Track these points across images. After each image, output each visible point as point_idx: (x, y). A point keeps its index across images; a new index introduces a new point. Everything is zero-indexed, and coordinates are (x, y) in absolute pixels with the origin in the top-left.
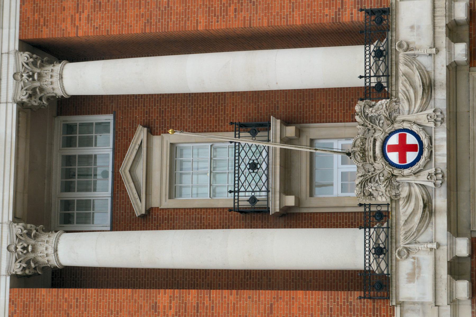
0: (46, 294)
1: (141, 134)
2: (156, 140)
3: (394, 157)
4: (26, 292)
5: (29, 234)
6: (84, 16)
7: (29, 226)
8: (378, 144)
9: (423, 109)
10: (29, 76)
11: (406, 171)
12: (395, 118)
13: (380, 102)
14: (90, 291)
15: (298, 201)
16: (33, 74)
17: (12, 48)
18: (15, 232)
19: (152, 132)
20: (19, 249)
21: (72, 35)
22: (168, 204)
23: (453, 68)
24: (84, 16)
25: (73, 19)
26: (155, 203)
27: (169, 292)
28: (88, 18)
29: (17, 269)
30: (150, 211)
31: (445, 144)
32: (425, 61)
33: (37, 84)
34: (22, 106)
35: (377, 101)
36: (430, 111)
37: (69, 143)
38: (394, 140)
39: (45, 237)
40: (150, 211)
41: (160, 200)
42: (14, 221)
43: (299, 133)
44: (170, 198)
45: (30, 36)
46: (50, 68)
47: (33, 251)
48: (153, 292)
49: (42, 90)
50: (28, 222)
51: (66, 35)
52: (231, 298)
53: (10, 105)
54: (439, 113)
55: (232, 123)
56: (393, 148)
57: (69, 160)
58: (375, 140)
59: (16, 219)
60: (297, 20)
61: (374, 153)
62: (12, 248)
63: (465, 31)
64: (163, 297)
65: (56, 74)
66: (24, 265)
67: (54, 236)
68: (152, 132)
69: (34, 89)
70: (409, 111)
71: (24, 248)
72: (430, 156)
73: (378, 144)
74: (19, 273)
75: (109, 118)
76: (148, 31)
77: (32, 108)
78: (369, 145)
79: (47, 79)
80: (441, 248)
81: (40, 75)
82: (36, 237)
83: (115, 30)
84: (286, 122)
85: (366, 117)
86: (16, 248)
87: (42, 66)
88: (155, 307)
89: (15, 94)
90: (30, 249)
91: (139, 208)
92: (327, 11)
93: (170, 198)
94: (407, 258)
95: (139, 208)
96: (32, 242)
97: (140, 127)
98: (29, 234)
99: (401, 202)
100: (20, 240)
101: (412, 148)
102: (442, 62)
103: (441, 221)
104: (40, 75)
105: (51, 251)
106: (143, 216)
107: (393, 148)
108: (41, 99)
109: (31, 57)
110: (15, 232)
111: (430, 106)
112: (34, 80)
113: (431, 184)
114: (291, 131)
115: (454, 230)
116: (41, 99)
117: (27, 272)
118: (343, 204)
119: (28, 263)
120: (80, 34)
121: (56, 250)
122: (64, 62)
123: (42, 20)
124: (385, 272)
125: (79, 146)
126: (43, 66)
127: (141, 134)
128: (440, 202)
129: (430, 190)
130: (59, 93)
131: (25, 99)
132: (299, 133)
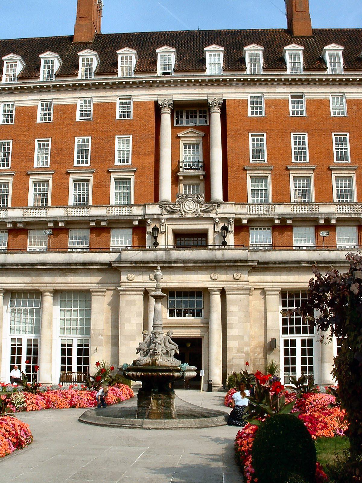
2: (201, 139)
15: (181, 180)
29: (159, 102)
43: (201, 180)
82: (169, 107)
98: (219, 104)
114: (201, 177)
132: (201, 180)
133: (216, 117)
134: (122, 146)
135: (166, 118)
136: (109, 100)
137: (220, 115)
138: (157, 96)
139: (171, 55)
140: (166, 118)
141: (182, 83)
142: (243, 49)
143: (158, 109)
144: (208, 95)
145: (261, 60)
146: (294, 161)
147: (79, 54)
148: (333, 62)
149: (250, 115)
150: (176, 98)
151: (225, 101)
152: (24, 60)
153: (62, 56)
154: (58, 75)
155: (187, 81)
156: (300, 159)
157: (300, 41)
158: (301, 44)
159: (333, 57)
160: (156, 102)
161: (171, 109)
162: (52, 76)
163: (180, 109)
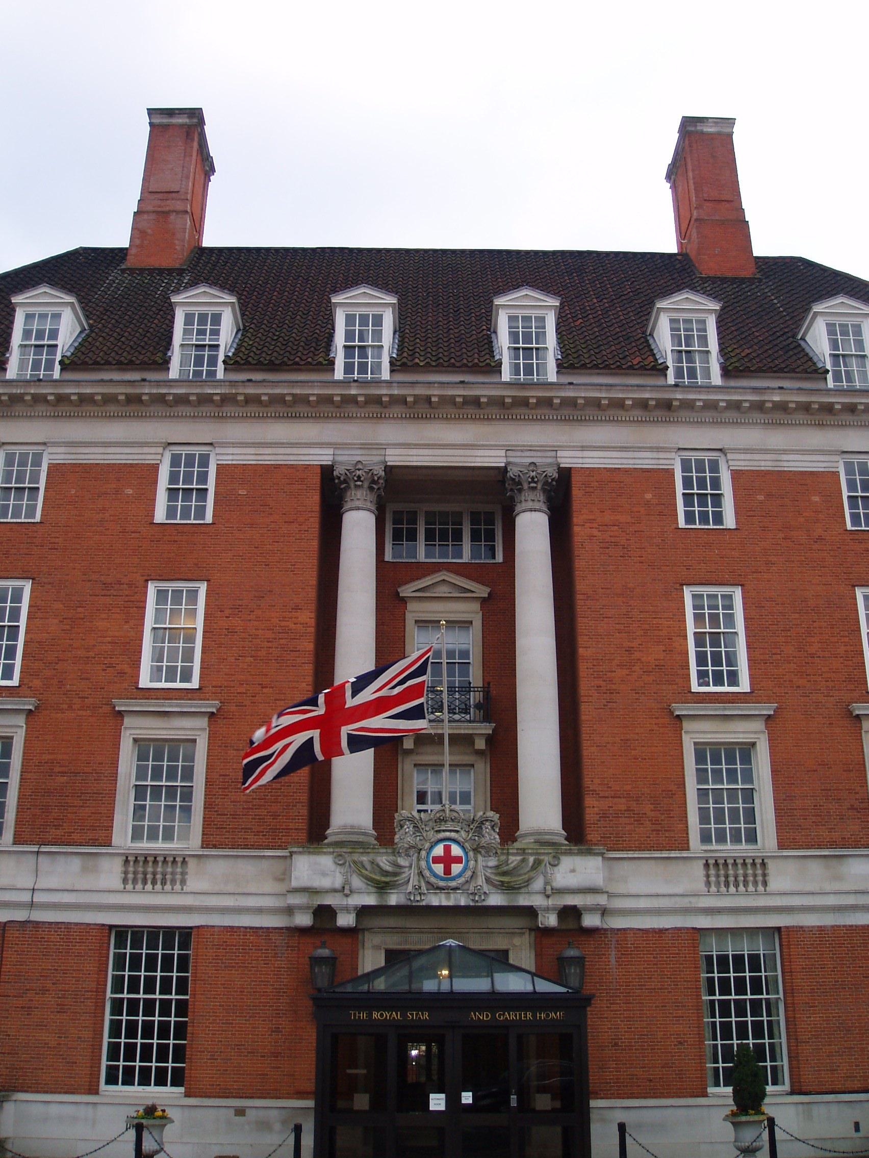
0: (314, 499)
1: (483, 591)
2: (476, 606)
3: (439, 851)
4: (316, 480)
5: (373, 482)
6: (595, 532)
7: (381, 481)
8: (453, 835)
9: (488, 880)
10: (533, 478)
11: (423, 864)
12: (480, 852)
13: (497, 837)
14: (315, 544)
15: (409, 752)
16: (535, 482)
17: (387, 459)
18: (549, 470)
19: (484, 601)
20: (358, 473)
21: (575, 520)
22: (410, 619)
23: (531, 912)
24: (595, 532)
25: (592, 521)
26: (411, 606)
27: (313, 622)
28: (591, 537)
29: (339, 471)
30: (404, 601)
31: (451, 903)
32: (538, 884)
33: (526, 486)
34: (504, 470)
35: (498, 834)
36: (486, 888)
37: (475, 518)
38: (456, 851)
39: (372, 497)
40: (404, 601)
41: (415, 612)
42: (386, 467)
43: (479, 753)
44: (416, 622)
45: (575, 479)
46: (542, 498)
47: (356, 486)
48: (313, 607)
49: (520, 491)
50: (386, 481)
51: (575, 514)
52: (304, 685)
53: (331, 458)
54: (483, 897)
55: (489, 684)
56: (447, 849)
57: (457, 519)
58: (457, 831)
59: (389, 469)
60: (589, 751)
61: (444, 831)
62: (360, 466)
63: (571, 925)
64: (308, 617)
65: (537, 505)
66: (342, 479)
67: (373, 508)
68: (484, 601)
69: (520, 483)
70: (487, 867)
71: (359, 477)
72: (439, 888)
73: (453, 835)
74: (335, 473)
75: (500, 558)
76: (578, 597)
77: (503, 482)
78: (449, 826)
79: (530, 495)
80: (345, 899)
81: (534, 488)
82: (371, 489)
83: (581, 563)
84: (490, 739)
85: (482, 823)
86: (359, 470)
87: (544, 490)
88: (297, 608)
89: (341, 463)
90: (359, 483)
91: (406, 591)
92: (597, 781)
93: (416, 622)
94: (336, 863)
95: (406, 591)
96: (366, 485)
97: (488, 590)
98: (373, 482)
99: (391, 858)
100: (367, 473)
101: (447, 871)
102: (537, 901)
103: (371, 900)
104: (534, 488)
105: (530, 505)
106: (398, 593)
107: (447, 849)
108: (512, 490)
109: (553, 480)
110: (549, 470)
111: (491, 887)
112: (530, 483)
113: (410, 888)
114: (480, 744)
115: (363, 912)
116: (512, 490)
117: (337, 481)
118: (405, 798)
119: (345, 481)
120: (576, 529)
121: (358, 509)
122: (376, 512)
123: (592, 490)
124: (326, 841)
125: (472, 529)
126: (544, 492)
127: (483, 591)
128: (393, 899)
129: (404, 887)
130: (518, 508)
131: (510, 474)
132: (479, 753)
133: (533, 530)
134: (172, 628)
135: (359, 529)
136: (645, 460)
137: (546, 518)
138: (331, 451)
139: (704, 322)
140: (359, 529)
141: (423, 409)
142: (492, 302)
143: (332, 491)
144: (338, 452)
145: (551, 340)
146: (695, 687)
147: (175, 299)
148: (684, 348)
149: (682, 523)
150: (395, 458)
151: (565, 474)
152: (83, 309)
153: (85, 302)
154: (73, 363)
155: (342, 401)
156: (718, 681)
157: (710, 286)
158: (715, 296)
159: (685, 335)
160: (327, 472)
161: (379, 496)
162: (50, 365)
163: (405, 499)
